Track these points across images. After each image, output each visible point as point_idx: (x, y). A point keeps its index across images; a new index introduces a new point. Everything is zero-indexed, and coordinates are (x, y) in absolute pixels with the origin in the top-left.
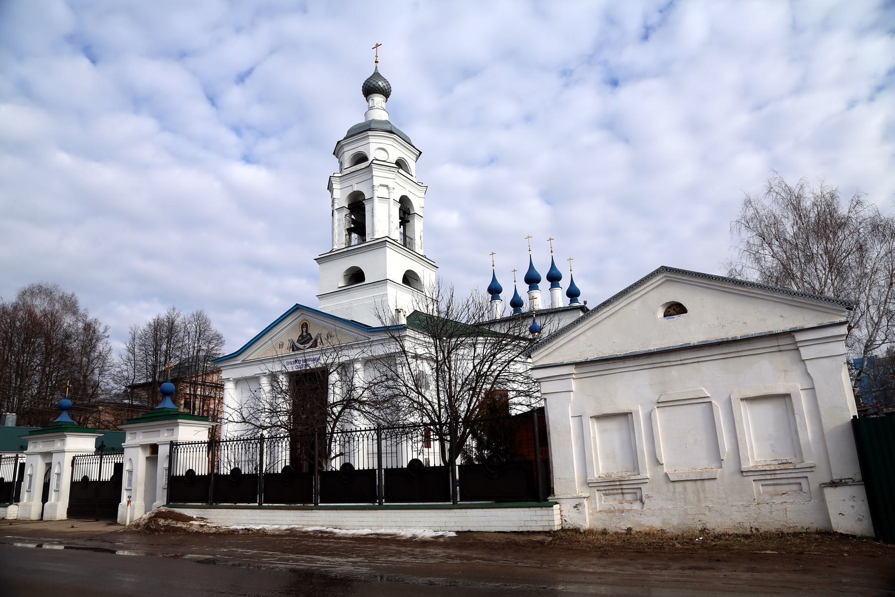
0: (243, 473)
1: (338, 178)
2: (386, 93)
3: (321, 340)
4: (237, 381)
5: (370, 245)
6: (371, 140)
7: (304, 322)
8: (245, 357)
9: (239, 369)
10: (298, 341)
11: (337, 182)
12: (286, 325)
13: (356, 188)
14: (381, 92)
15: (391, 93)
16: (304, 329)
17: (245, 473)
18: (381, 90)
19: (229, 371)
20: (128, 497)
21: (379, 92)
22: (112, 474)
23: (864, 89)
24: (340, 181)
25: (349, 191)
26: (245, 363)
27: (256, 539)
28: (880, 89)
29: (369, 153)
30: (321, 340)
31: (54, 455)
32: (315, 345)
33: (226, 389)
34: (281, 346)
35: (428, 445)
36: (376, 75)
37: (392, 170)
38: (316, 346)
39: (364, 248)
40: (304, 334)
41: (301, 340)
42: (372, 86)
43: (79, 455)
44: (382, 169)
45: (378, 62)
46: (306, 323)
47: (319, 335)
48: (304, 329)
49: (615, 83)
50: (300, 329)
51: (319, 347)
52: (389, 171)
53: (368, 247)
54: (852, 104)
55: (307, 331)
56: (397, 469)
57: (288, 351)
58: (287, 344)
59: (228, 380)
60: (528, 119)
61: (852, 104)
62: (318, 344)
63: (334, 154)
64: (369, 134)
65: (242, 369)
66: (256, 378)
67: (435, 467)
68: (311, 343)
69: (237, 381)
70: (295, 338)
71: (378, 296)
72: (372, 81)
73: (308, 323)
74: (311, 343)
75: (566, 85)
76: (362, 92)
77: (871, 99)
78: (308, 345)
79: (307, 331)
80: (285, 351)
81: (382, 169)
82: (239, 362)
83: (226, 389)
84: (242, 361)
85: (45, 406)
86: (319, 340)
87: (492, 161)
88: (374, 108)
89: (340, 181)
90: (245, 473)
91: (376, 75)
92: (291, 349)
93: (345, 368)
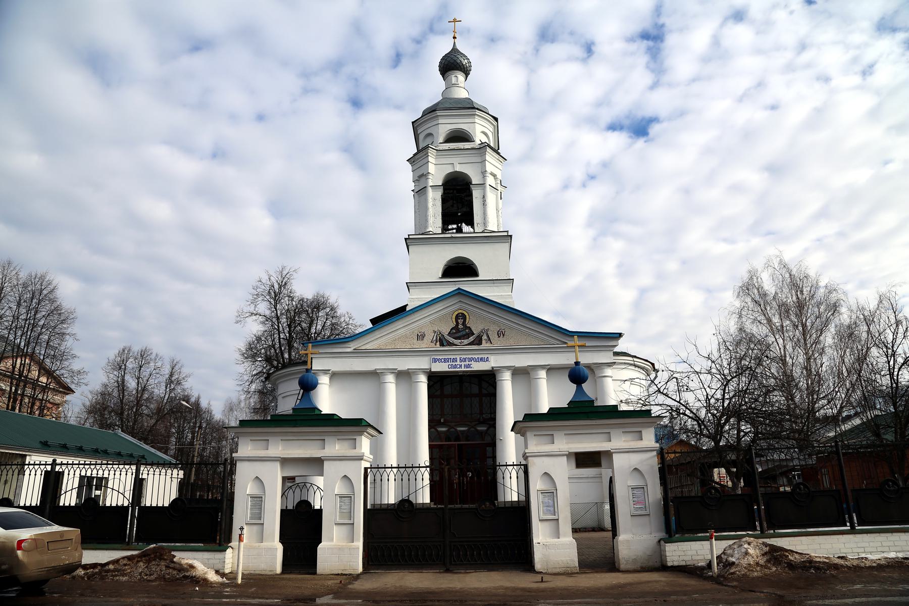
0: (61, 504)
1: (435, 151)
2: (466, 72)
3: (488, 336)
4: (335, 376)
8: (359, 346)
9: (344, 359)
12: (435, 311)
13: (458, 168)
15: (471, 72)
16: (459, 321)
17: (64, 504)
20: (240, 529)
21: (459, 69)
24: (437, 155)
25: (449, 170)
26: (358, 353)
27: (195, 600)
29: (475, 133)
33: (321, 384)
34: (420, 337)
35: (52, 478)
36: (454, 50)
37: (500, 160)
38: (480, 343)
39: (482, 239)
40: (460, 326)
42: (452, 61)
43: (38, 462)
45: (456, 38)
47: (486, 332)
48: (460, 321)
50: (454, 320)
51: (485, 345)
52: (498, 159)
54: (566, 187)
55: (464, 324)
56: (157, 507)
57: (433, 344)
58: (430, 336)
59: (325, 372)
60: (261, 118)
61: (566, 187)
62: (484, 342)
63: (413, 123)
64: (477, 113)
66: (376, 375)
67: (111, 507)
68: (471, 339)
70: (446, 329)
74: (471, 339)
76: (439, 64)
78: (466, 341)
79: (464, 324)
83: (321, 384)
84: (354, 349)
85: (24, 377)
86: (485, 337)
87: (218, 154)
88: (457, 85)
89: (437, 155)
90: (64, 504)
91: (454, 50)
92: (438, 343)
93: (522, 374)
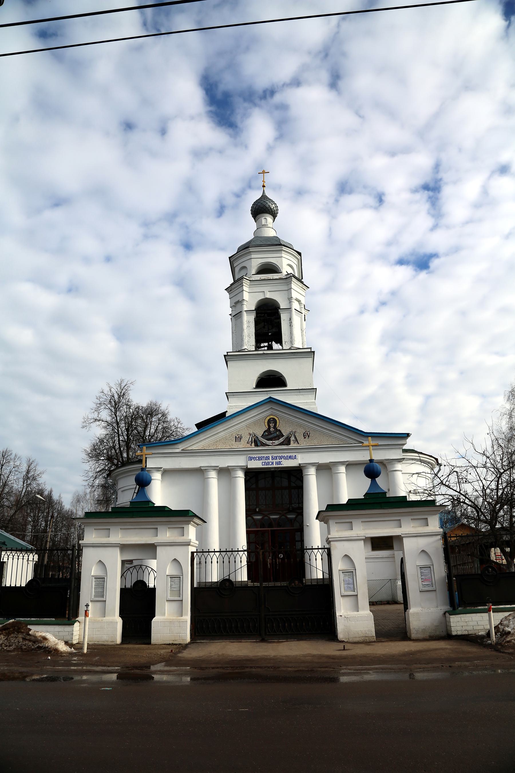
3: (295, 438)
4: (165, 472)
5: (295, 353)
6: (283, 255)
7: (272, 417)
9: (173, 459)
10: (263, 436)
11: (247, 284)
13: (268, 295)
14: (270, 212)
16: (271, 425)
18: (270, 211)
19: (158, 459)
20: (86, 606)
22: (30, 578)
23: (372, 302)
25: (261, 297)
26: (185, 453)
28: (383, 304)
29: (282, 266)
30: (295, 438)
31: (159, 549)
32: (287, 442)
34: (238, 439)
37: (304, 288)
41: (267, 435)
42: (262, 206)
44: (297, 284)
46: (274, 419)
48: (272, 425)
49: (188, 246)
51: (293, 445)
52: (302, 287)
53: (292, 354)
55: (275, 427)
57: (249, 445)
58: (246, 438)
59: (158, 469)
60: (108, 259)
62: (292, 442)
63: (230, 258)
64: (283, 249)
65: (179, 459)
66: (200, 471)
68: (281, 440)
69: (165, 472)
70: (259, 432)
71: (304, 403)
72: (262, 202)
73: (277, 419)
74: (281, 440)
75: (146, 237)
77: (377, 310)
78: (277, 442)
79: (275, 427)
80: (242, 445)
81: (297, 284)
82: (177, 451)
84: (182, 450)
86: (293, 438)
88: (267, 226)
89: (249, 287)
92: (253, 444)
